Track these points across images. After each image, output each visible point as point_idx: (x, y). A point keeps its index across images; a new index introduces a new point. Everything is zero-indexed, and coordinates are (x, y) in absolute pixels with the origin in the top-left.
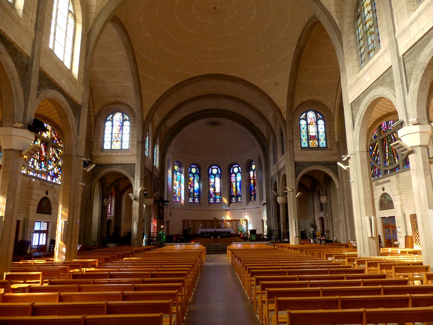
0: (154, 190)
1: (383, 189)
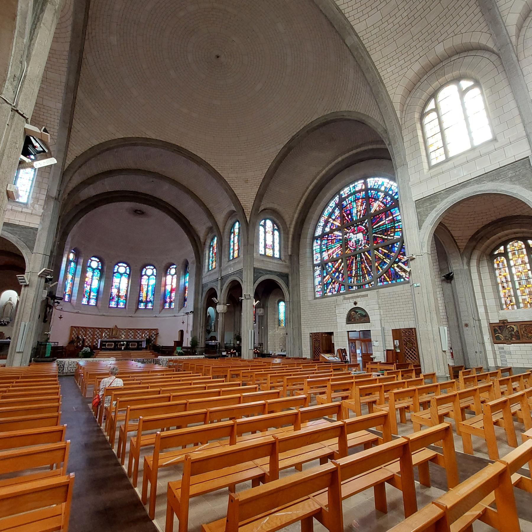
1: (355, 303)
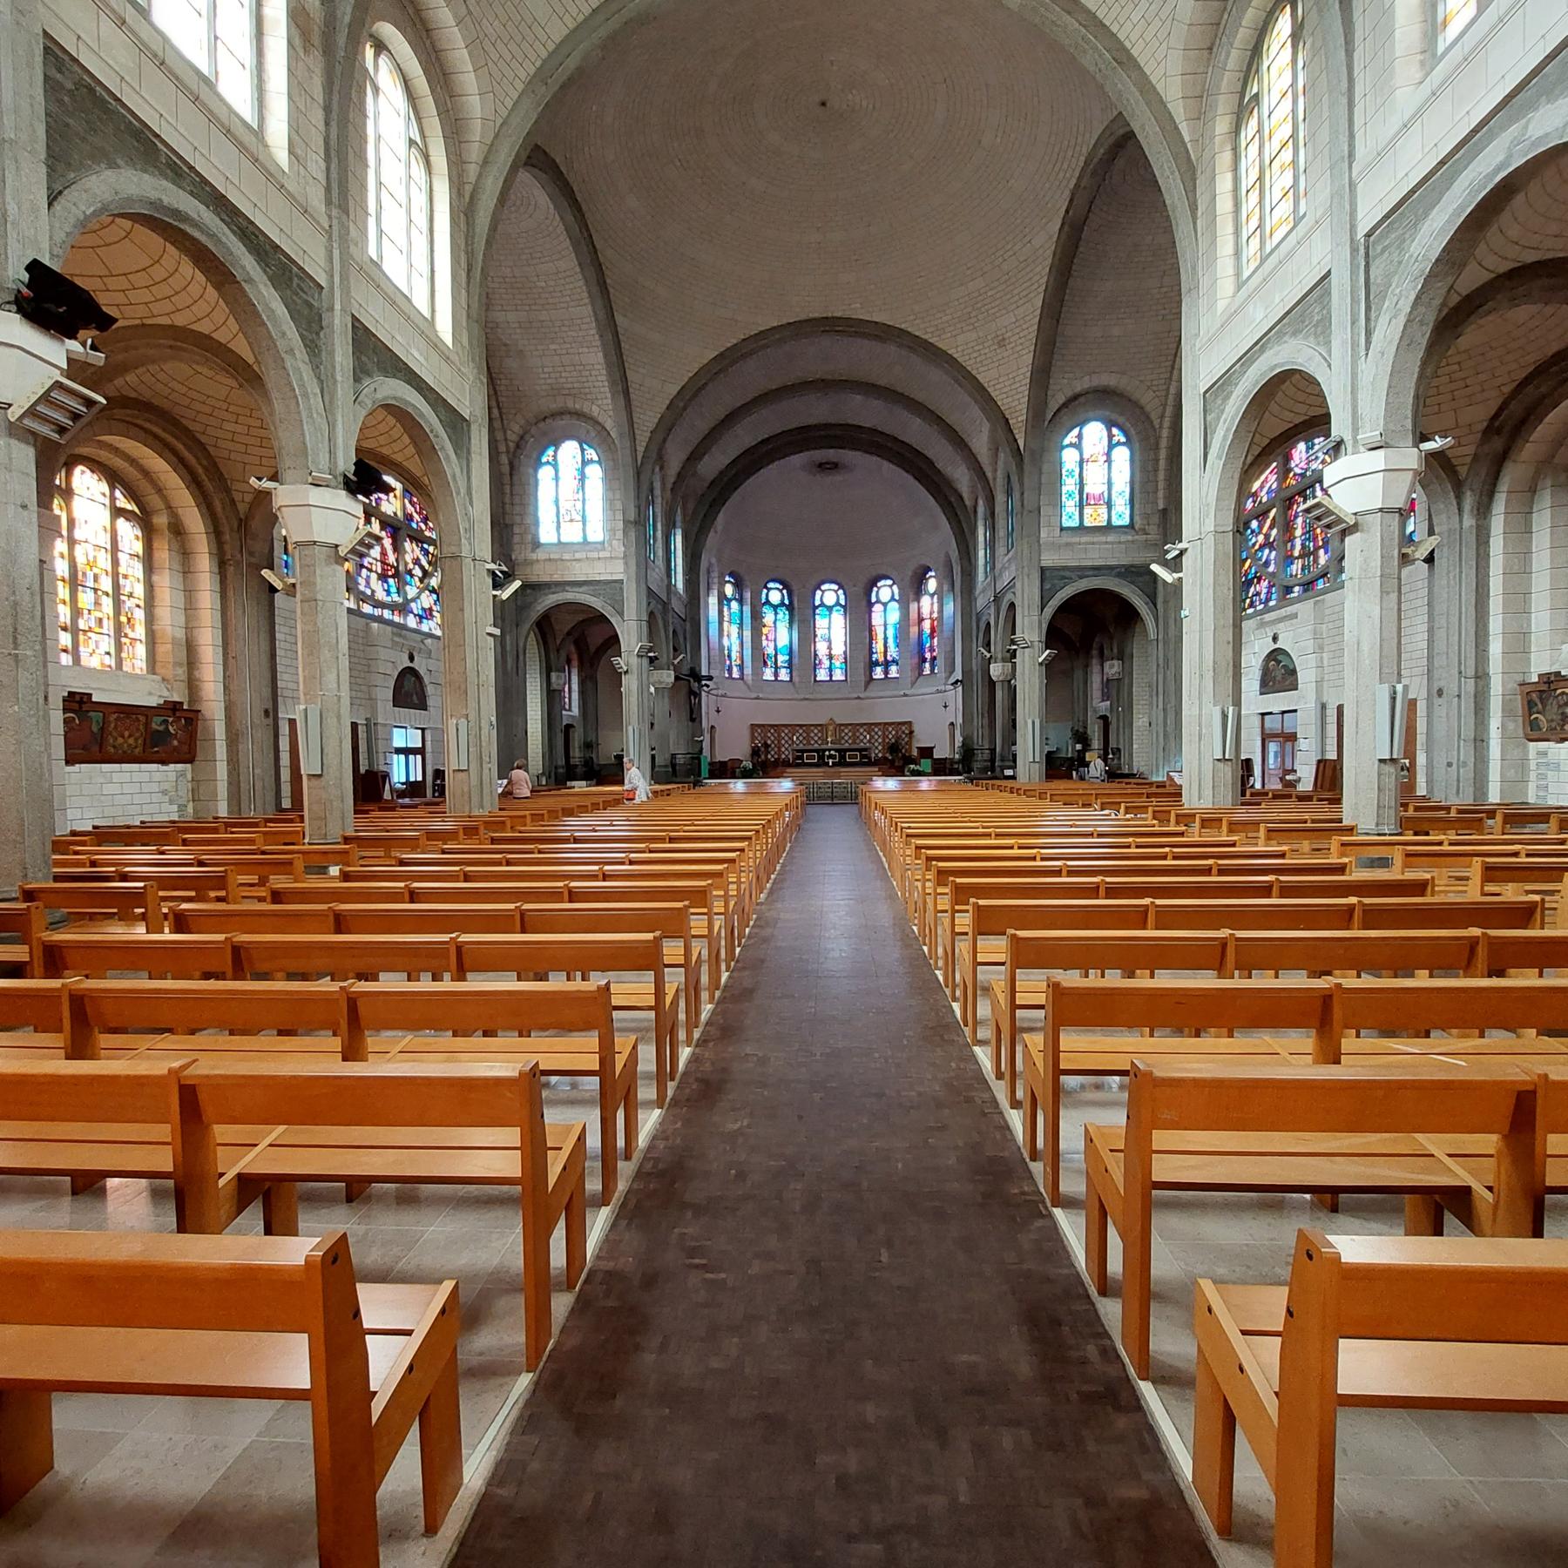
0: (675, 649)
1: (1275, 639)
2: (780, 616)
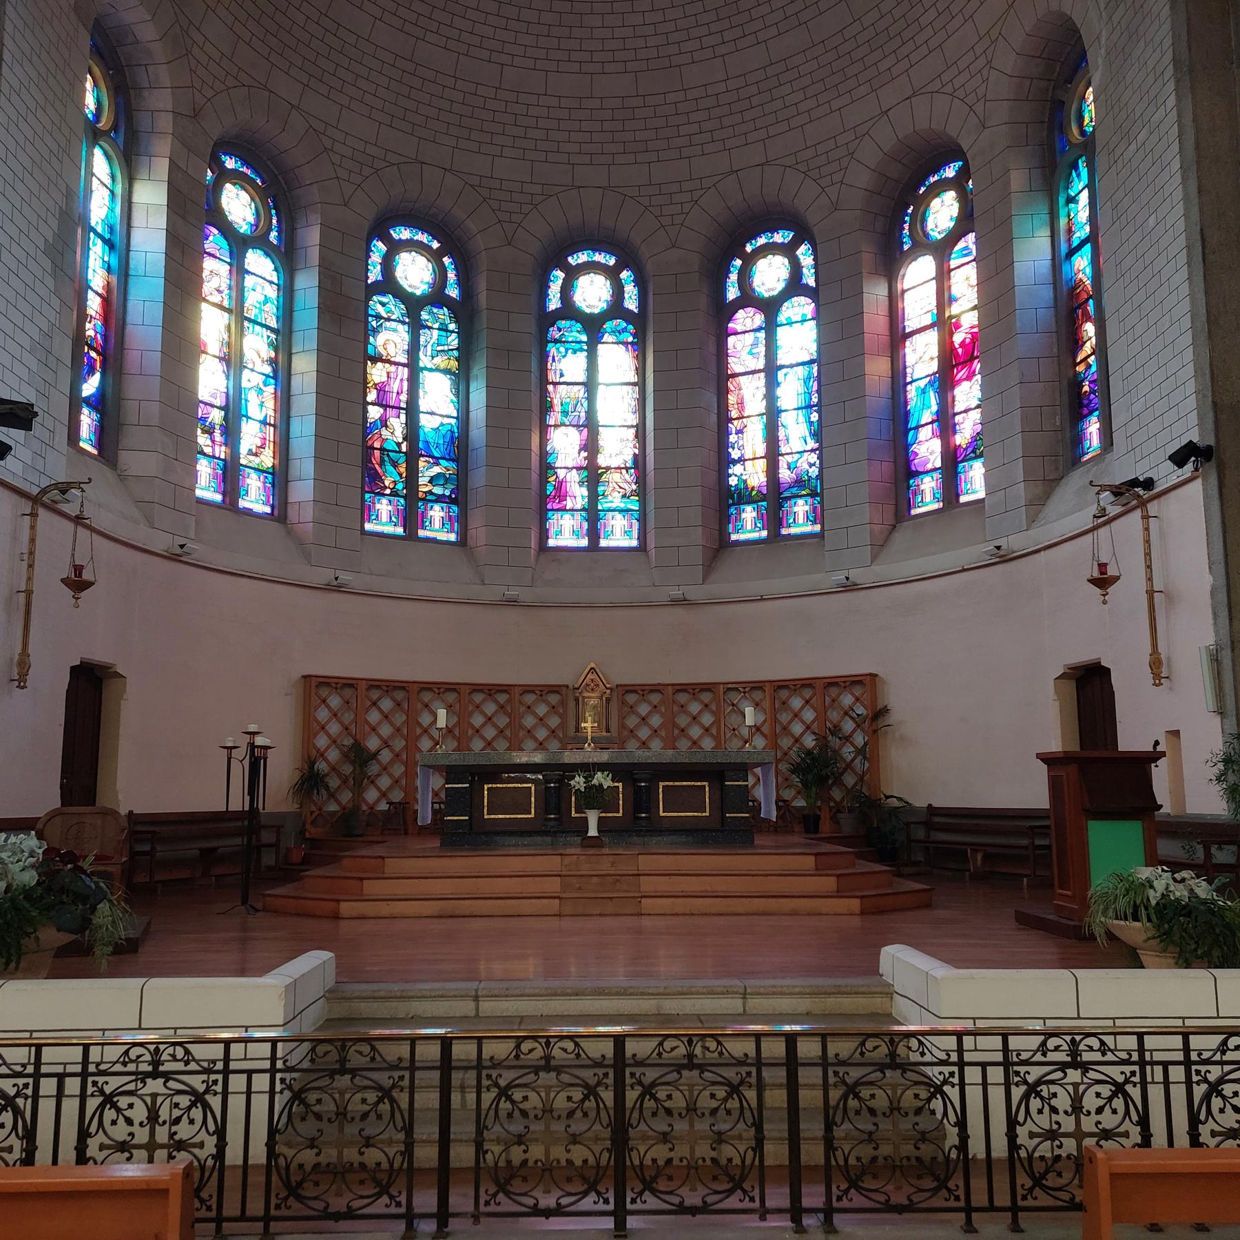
2: (429, 338)
